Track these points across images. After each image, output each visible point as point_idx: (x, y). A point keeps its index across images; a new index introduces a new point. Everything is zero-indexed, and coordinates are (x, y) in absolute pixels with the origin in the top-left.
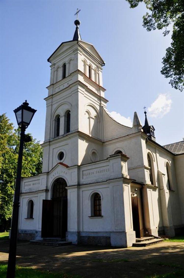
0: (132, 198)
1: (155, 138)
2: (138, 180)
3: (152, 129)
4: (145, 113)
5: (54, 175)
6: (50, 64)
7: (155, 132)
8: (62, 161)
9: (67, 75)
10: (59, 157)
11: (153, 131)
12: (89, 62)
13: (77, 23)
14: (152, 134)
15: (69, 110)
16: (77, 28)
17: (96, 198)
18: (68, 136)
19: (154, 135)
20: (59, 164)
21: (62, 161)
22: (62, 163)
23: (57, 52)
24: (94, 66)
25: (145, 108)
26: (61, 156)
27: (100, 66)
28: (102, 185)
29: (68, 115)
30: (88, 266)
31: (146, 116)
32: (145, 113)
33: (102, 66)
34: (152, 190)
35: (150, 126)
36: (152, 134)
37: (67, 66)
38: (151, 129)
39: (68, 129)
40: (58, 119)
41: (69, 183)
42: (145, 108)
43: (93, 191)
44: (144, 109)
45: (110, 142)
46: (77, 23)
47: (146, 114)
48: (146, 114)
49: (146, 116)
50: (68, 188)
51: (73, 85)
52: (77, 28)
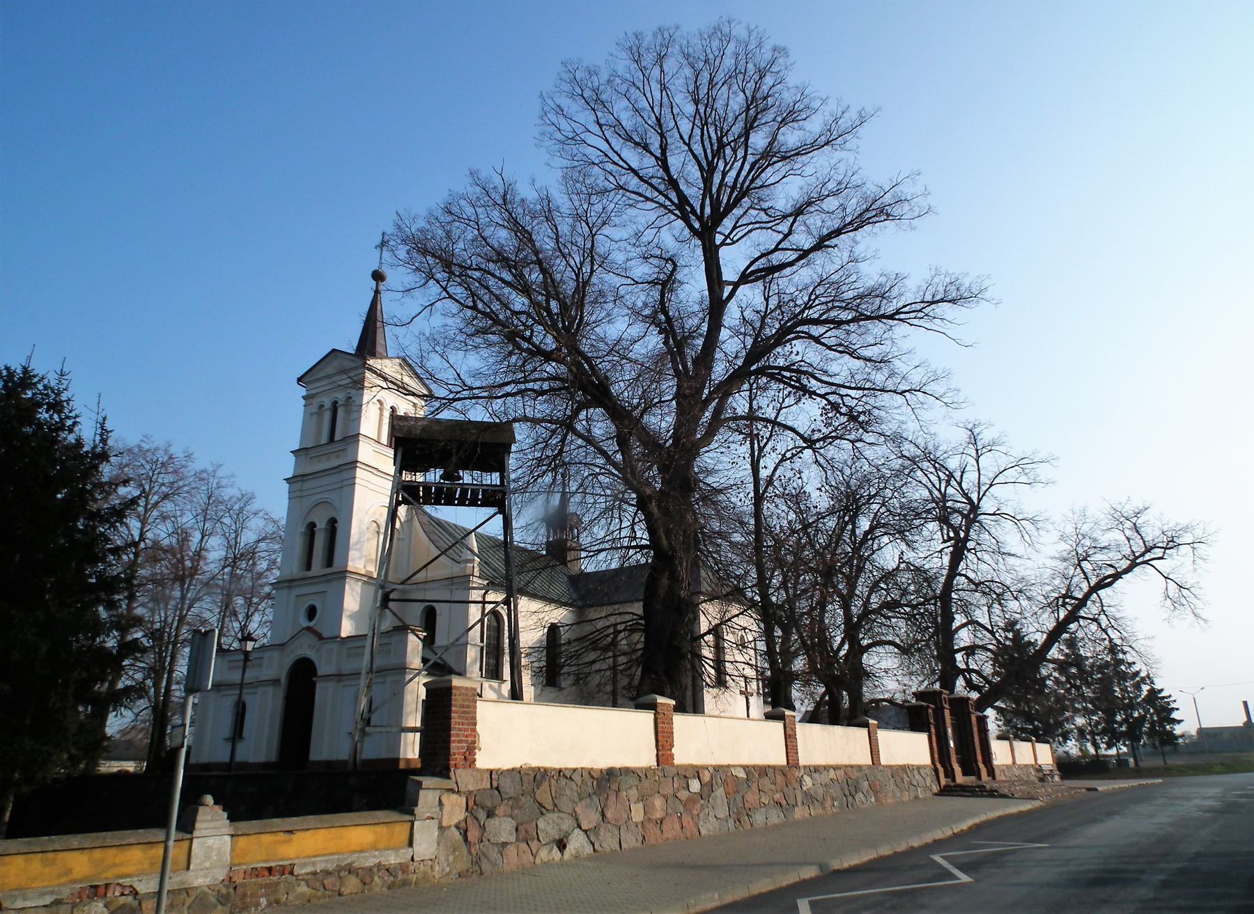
6: (303, 392)
8: (311, 624)
9: (338, 437)
16: (377, 292)
21: (311, 624)
23: (320, 365)
29: (333, 523)
37: (340, 411)
39: (329, 561)
40: (312, 526)
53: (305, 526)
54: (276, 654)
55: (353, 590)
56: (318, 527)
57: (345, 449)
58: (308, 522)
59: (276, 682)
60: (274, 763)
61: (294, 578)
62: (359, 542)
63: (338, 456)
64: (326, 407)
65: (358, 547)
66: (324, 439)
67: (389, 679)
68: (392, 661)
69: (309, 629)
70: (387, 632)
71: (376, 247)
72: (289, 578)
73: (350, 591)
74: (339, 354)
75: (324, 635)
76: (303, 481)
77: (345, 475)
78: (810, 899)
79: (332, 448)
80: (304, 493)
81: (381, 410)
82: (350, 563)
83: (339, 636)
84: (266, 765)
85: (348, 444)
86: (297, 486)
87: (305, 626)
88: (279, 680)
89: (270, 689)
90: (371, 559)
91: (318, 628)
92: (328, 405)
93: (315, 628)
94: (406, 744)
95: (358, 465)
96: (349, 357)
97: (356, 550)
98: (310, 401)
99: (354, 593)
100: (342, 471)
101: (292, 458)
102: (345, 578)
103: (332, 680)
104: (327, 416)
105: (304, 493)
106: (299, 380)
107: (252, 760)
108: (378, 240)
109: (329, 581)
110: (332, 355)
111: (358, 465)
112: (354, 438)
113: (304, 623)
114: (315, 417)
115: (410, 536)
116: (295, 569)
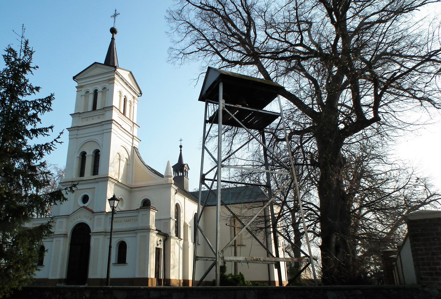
0: (156, 248)
1: (188, 179)
2: (163, 231)
3: (186, 168)
4: (181, 147)
5: (74, 219)
6: (76, 84)
7: (189, 171)
8: (86, 205)
9: (98, 108)
10: (82, 199)
11: (186, 170)
12: (125, 93)
13: (113, 31)
14: (185, 175)
15: (99, 151)
16: (113, 39)
17: (122, 246)
18: (96, 179)
19: (187, 176)
20: (82, 208)
21: (86, 205)
22: (86, 207)
23: (87, 70)
24: (129, 98)
25: (181, 140)
26: (85, 199)
27: (136, 97)
28: (129, 234)
29: (97, 154)
30: (308, 127)
31: (181, 151)
32: (181, 147)
33: (138, 96)
34: (239, 61)
35: (184, 165)
36: (185, 175)
37: (99, 95)
38: (185, 168)
39: (95, 171)
40: (83, 155)
41: (94, 229)
42: (181, 140)
43: (119, 240)
44: (180, 142)
45: (137, 189)
46: (113, 31)
47: (181, 149)
48: (181, 149)
49: (181, 151)
50: (92, 234)
51: (88, 85)
52: (113, 39)
53: (79, 154)
54: (64, 220)
55: (111, 187)
56: (87, 154)
57: (104, 114)
58: (80, 152)
59: (65, 235)
60: (65, 279)
61: (74, 180)
62: (113, 163)
63: (99, 118)
64: (90, 92)
65: (113, 165)
66: (90, 108)
67: (139, 235)
68: (140, 224)
69: (84, 207)
70: (137, 209)
71: (111, 17)
72: (72, 181)
73: (110, 188)
74: (98, 65)
75: (94, 211)
76: (78, 130)
77: (105, 127)
78: (148, 287)
79: (95, 113)
80: (78, 137)
81: (120, 96)
82: (109, 173)
83: (105, 212)
84: (60, 281)
85: (106, 111)
86: (75, 132)
87: (81, 206)
88: (67, 235)
89: (62, 239)
90: (117, 173)
91: (89, 207)
92: (92, 91)
93: (89, 207)
94: (150, 270)
95: (113, 122)
96: (102, 66)
97: (112, 167)
98: (80, 89)
99: (111, 189)
100: (103, 125)
101: (71, 118)
102: (107, 180)
103: (101, 235)
104: (91, 98)
105: (78, 137)
106: (74, 78)
107: (51, 277)
108: (113, 13)
109: (97, 182)
110: (94, 66)
111: (113, 122)
112: (111, 108)
113: (82, 205)
114: (83, 97)
115: (133, 163)
116: (74, 175)
